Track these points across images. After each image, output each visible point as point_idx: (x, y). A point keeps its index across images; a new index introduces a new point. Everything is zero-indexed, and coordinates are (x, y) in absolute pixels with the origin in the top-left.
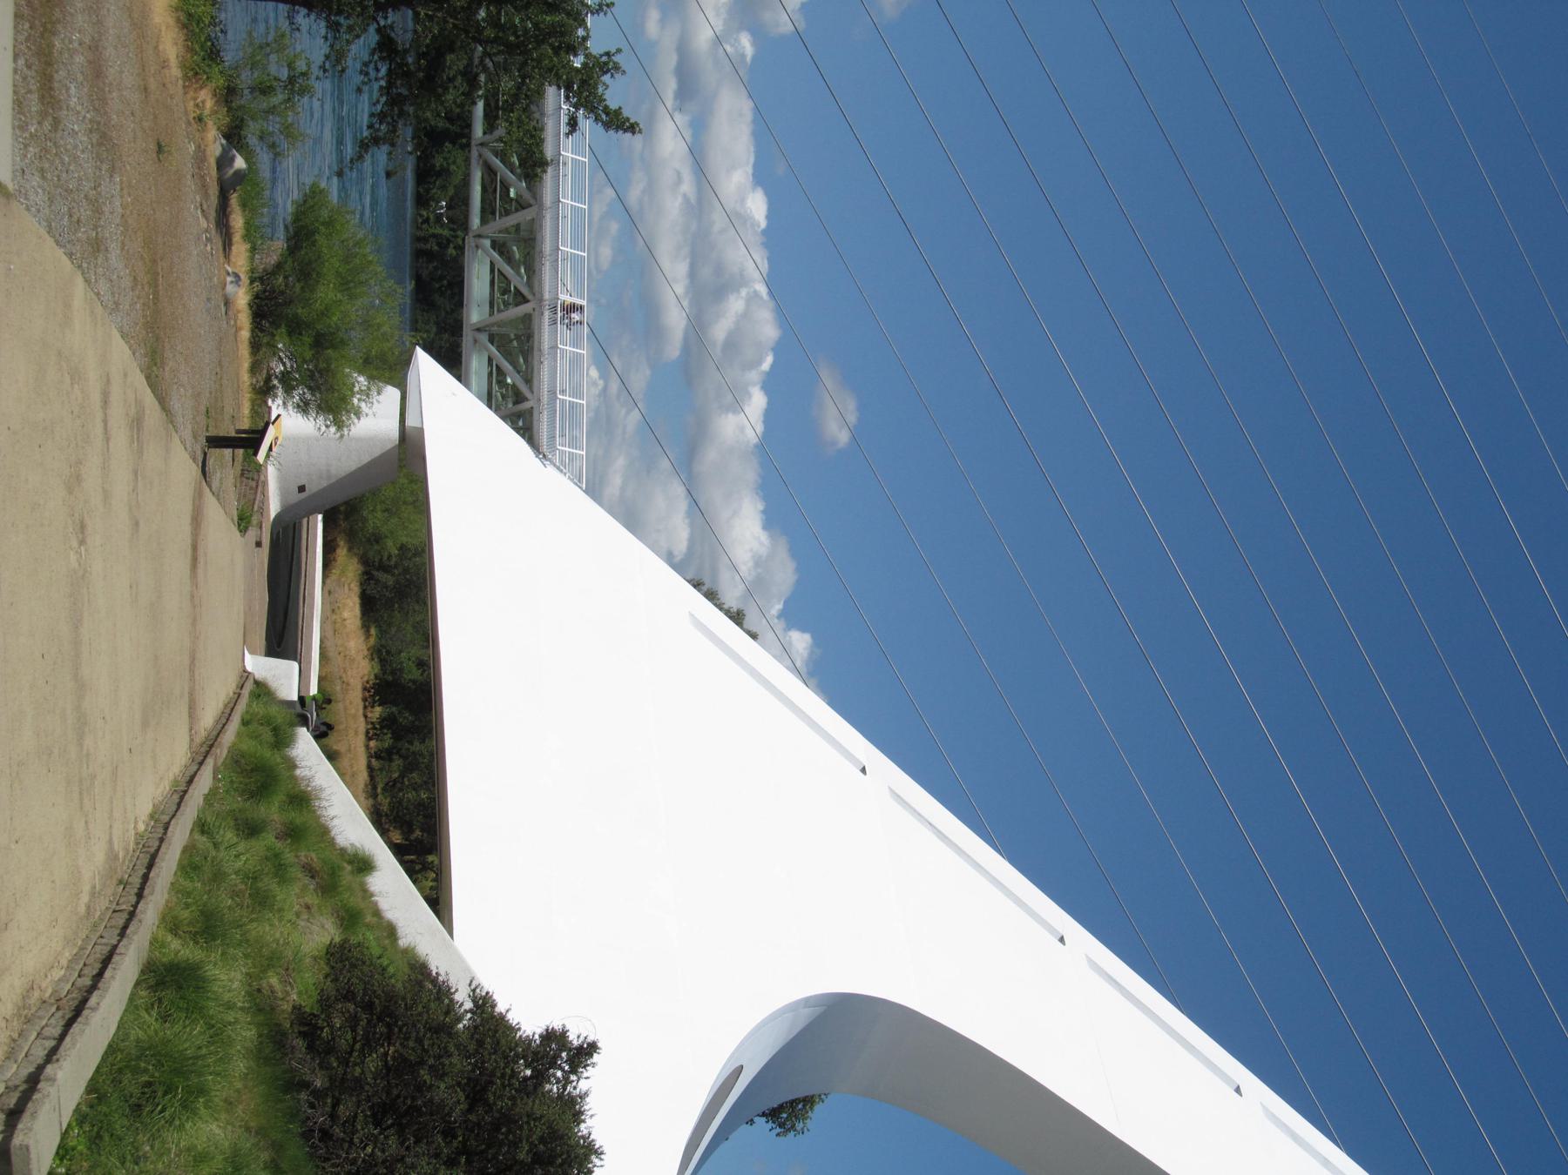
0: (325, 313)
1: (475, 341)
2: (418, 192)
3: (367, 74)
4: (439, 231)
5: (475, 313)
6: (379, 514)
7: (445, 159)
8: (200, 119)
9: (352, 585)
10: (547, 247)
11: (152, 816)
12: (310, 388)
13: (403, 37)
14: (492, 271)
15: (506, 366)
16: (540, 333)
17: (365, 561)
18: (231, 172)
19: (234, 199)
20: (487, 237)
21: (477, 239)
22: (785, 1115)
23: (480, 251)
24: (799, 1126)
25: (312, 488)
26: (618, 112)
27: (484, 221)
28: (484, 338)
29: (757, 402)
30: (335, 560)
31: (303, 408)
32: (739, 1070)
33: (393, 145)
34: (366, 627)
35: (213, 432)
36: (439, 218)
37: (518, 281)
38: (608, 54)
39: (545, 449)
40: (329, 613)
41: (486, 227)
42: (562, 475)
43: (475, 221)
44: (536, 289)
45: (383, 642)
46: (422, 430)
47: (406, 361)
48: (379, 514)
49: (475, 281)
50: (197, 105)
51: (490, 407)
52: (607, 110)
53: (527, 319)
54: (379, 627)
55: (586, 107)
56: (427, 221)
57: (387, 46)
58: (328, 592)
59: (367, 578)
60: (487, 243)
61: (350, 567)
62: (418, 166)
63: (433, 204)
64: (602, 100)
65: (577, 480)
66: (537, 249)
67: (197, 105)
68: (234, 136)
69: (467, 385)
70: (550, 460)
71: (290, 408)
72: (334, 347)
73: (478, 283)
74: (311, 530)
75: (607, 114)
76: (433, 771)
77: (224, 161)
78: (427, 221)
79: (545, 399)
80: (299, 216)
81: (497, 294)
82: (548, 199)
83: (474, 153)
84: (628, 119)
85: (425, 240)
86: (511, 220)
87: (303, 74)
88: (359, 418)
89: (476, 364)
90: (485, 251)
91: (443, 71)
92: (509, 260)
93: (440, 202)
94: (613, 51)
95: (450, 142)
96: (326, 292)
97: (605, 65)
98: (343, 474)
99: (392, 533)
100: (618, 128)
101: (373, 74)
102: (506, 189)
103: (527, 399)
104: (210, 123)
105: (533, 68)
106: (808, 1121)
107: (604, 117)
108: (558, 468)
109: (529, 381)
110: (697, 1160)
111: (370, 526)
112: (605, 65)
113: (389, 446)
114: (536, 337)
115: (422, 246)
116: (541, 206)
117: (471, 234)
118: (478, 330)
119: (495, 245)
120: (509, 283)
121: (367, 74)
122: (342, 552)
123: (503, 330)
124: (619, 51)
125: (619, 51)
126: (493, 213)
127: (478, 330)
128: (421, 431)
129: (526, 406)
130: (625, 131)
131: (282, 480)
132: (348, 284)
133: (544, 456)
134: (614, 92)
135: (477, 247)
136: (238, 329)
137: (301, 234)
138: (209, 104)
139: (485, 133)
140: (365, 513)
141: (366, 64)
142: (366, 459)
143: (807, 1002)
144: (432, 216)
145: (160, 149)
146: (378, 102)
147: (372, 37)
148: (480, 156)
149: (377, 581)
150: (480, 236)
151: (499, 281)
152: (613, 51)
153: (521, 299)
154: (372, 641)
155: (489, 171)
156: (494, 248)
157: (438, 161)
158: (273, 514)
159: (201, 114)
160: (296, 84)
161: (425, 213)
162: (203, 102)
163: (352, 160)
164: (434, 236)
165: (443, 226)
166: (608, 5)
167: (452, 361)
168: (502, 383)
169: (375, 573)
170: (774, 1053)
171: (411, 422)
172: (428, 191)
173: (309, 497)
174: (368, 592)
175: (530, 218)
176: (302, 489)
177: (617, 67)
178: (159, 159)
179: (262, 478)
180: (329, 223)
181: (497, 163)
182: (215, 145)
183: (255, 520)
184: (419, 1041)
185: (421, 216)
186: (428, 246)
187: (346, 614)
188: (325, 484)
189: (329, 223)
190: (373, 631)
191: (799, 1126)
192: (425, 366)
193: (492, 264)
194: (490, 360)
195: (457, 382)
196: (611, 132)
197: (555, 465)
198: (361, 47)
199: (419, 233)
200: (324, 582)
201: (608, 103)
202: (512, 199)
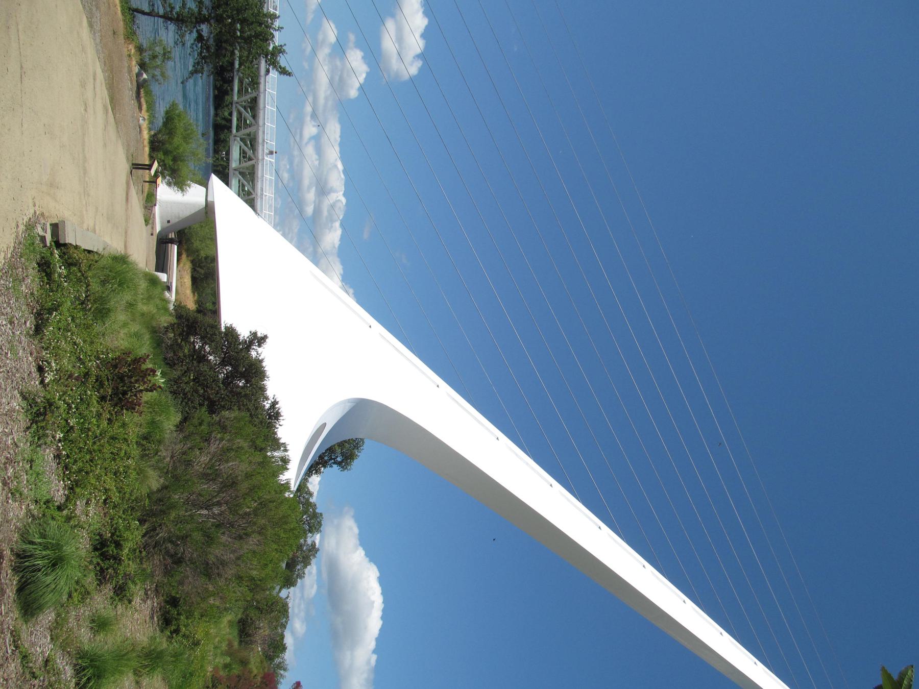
0: (177, 148)
1: (234, 174)
2: (214, 148)
3: (193, 48)
4: (222, 163)
5: (234, 164)
6: (198, 242)
7: (225, 136)
8: (129, 56)
9: (188, 271)
10: (260, 175)
11: (102, 72)
12: (171, 178)
13: (205, 34)
14: (240, 149)
15: (245, 183)
16: (257, 171)
17: (192, 262)
18: (142, 79)
19: (142, 91)
20: (238, 137)
21: (234, 171)
22: (343, 464)
23: (236, 142)
24: (349, 467)
25: (172, 222)
26: (284, 68)
27: (238, 130)
28: (237, 173)
29: (339, 232)
30: (181, 259)
31: (169, 184)
32: (324, 425)
33: (202, 74)
34: (193, 292)
35: (134, 162)
36: (222, 158)
37: (250, 153)
38: (281, 46)
39: (259, 212)
40: (179, 278)
41: (239, 133)
42: (265, 222)
43: (234, 131)
44: (256, 155)
45: (200, 299)
46: (213, 202)
47: (208, 179)
48: (198, 242)
49: (234, 152)
50: (128, 50)
51: (239, 196)
52: (280, 67)
53: (253, 166)
54: (198, 294)
55: (273, 65)
56: (218, 159)
57: (200, 38)
58: (179, 271)
59: (194, 270)
60: (239, 139)
61: (188, 266)
62: (214, 138)
63: (220, 152)
64: (278, 63)
65: (270, 223)
66: (257, 141)
67: (128, 50)
68: (143, 66)
69: (231, 188)
70: (260, 216)
71: (164, 183)
72: (181, 161)
73: (235, 153)
74: (172, 250)
75: (281, 69)
76: (215, 291)
77: (139, 75)
78: (218, 159)
79: (259, 194)
80: (167, 112)
81: (242, 158)
82: (261, 123)
83: (234, 106)
84: (288, 71)
85: (217, 166)
86: (247, 131)
87: (169, 52)
88: (190, 188)
89: (234, 182)
90: (238, 141)
91: (224, 102)
92: (246, 145)
93: (222, 152)
94: (283, 45)
95: (227, 129)
96: (177, 140)
97: (279, 50)
98: (184, 217)
99: (203, 248)
100: (284, 74)
101: (195, 48)
102: (245, 121)
103: (252, 194)
104: (134, 59)
105: (254, 45)
106: (352, 466)
107: (279, 69)
108: (264, 219)
109: (253, 189)
110: (313, 454)
111: (195, 245)
112: (279, 50)
113: (201, 207)
114: (256, 173)
115: (215, 168)
116: (258, 126)
117: (233, 135)
118: (235, 170)
119: (242, 140)
120: (246, 154)
121: (193, 48)
122: (184, 256)
123: (244, 171)
124: (285, 45)
125: (285, 45)
126: (241, 127)
127: (235, 170)
128: (213, 202)
129: (253, 196)
130: (287, 75)
131: (161, 218)
132: (186, 138)
133: (259, 215)
134: (282, 61)
135: (235, 140)
136: (144, 146)
137: (169, 119)
138: (133, 51)
139: (238, 99)
140: (193, 241)
141: (193, 44)
142: (193, 212)
143: (349, 401)
144: (220, 158)
145: (114, 33)
146: (197, 58)
147: (195, 35)
148: (236, 107)
149: (198, 272)
150: (235, 136)
151: (243, 154)
152: (283, 45)
153: (250, 159)
154: (196, 297)
155: (240, 113)
156: (241, 141)
157: (222, 137)
158: (158, 231)
159: (130, 53)
160: (166, 56)
161: (217, 156)
162: (131, 50)
163: (187, 78)
164: (220, 165)
165: (224, 161)
166: (281, 28)
167: (226, 180)
168: (243, 190)
169: (197, 269)
170: (338, 419)
171: (209, 199)
172: (218, 148)
173: (172, 225)
174: (194, 275)
175: (254, 131)
176: (169, 222)
177: (284, 51)
178: (114, 38)
179: (153, 212)
180: (179, 116)
181: (242, 110)
182: (136, 69)
183: (150, 222)
184: (205, 329)
185: (216, 157)
186: (218, 169)
187: (186, 280)
188: (177, 220)
189: (179, 116)
190: (196, 294)
191: (349, 467)
192: (215, 180)
193: (240, 147)
194: (239, 181)
195: (226, 187)
196: (282, 76)
197: (262, 218)
198: (190, 38)
199: (215, 164)
200: (177, 267)
201: (281, 64)
202: (248, 124)
